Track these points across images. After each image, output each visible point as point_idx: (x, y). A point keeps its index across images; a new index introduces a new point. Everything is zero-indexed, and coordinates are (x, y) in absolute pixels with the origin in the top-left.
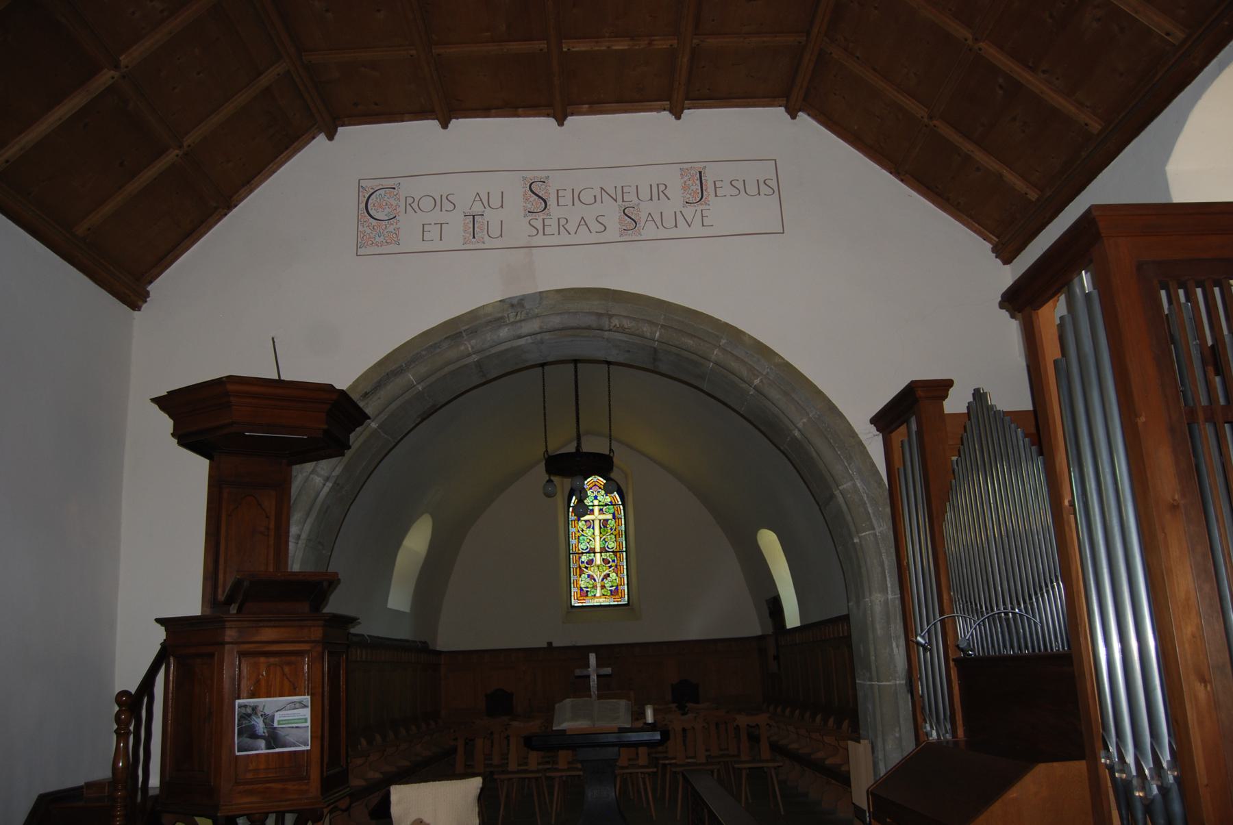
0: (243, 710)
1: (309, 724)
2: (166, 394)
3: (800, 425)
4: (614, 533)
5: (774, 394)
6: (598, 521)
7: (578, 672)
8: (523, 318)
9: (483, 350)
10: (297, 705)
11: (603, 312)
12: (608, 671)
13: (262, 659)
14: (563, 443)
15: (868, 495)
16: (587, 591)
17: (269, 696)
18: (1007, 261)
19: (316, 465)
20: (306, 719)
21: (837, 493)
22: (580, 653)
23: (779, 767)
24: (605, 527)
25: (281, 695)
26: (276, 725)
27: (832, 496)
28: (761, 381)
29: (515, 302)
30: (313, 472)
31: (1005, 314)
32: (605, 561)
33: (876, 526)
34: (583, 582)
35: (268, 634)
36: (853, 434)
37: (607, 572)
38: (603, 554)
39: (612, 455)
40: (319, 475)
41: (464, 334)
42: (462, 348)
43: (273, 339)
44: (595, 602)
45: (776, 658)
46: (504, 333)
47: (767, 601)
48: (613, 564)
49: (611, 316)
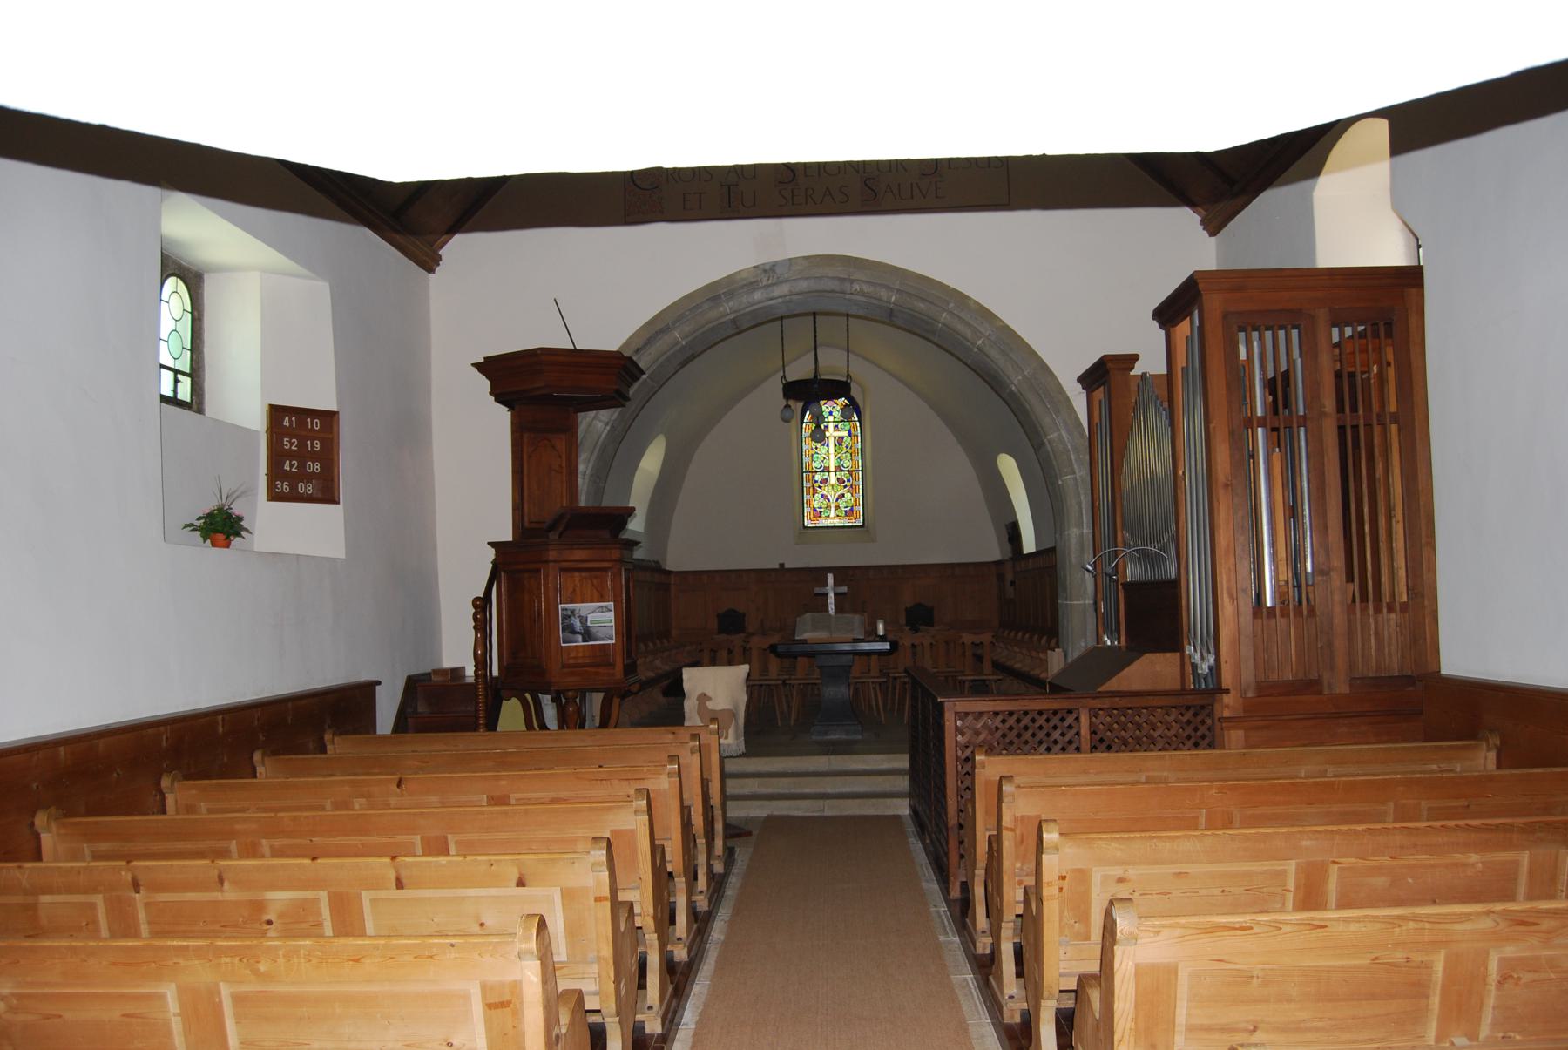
0: (565, 612)
1: (613, 624)
2: (483, 360)
3: (1016, 382)
4: (850, 451)
5: (994, 354)
6: (833, 439)
7: (817, 590)
8: (774, 282)
9: (740, 310)
10: (604, 609)
11: (846, 277)
12: (844, 589)
13: (577, 574)
14: (800, 370)
15: (1071, 444)
16: (821, 512)
17: (583, 602)
18: (1213, 234)
19: (596, 414)
20: (611, 620)
21: (1045, 440)
22: (818, 574)
23: (1000, 680)
24: (840, 444)
25: (592, 602)
26: (589, 624)
27: (1042, 444)
28: (983, 342)
29: (767, 267)
30: (594, 418)
31: (1155, 324)
32: (840, 481)
33: (1077, 471)
34: (817, 502)
35: (579, 554)
36: (1061, 391)
37: (842, 492)
38: (838, 473)
39: (849, 381)
40: (600, 421)
41: (723, 296)
42: (721, 309)
43: (555, 300)
44: (829, 523)
45: (1013, 583)
46: (758, 295)
47: (1006, 526)
48: (849, 484)
49: (852, 281)
